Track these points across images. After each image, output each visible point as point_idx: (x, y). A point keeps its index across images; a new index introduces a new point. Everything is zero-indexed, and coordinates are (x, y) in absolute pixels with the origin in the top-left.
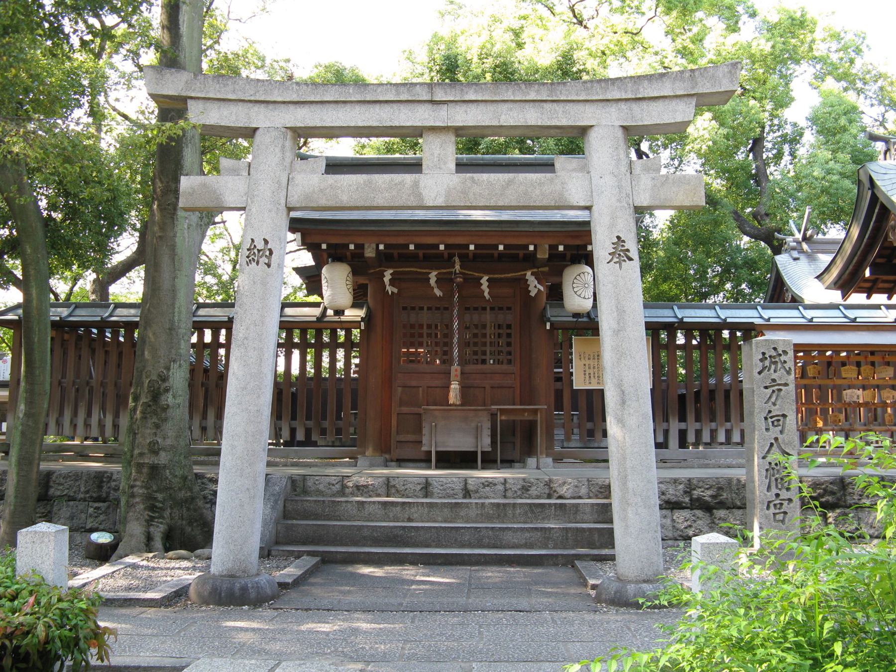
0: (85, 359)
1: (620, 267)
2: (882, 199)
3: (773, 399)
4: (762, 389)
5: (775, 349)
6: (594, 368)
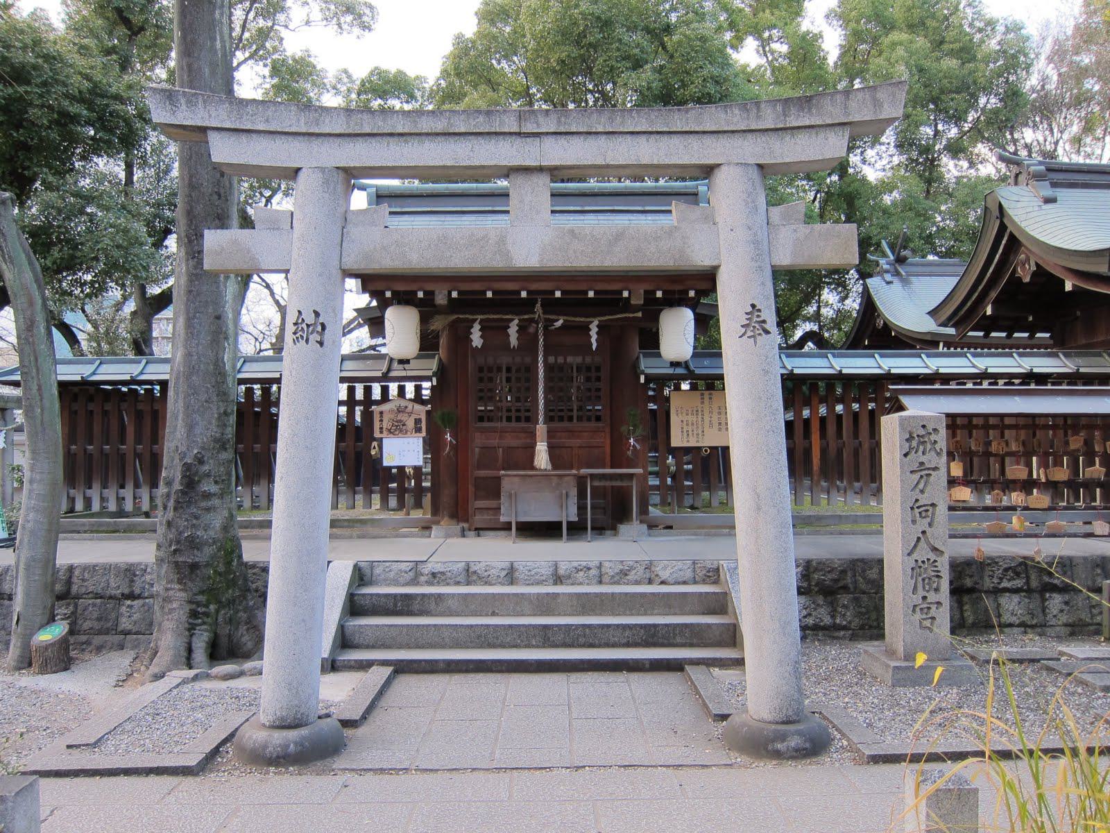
0: (105, 433)
1: (755, 342)
2: (1010, 228)
3: (921, 486)
4: (908, 473)
5: (924, 426)
6: (693, 424)
